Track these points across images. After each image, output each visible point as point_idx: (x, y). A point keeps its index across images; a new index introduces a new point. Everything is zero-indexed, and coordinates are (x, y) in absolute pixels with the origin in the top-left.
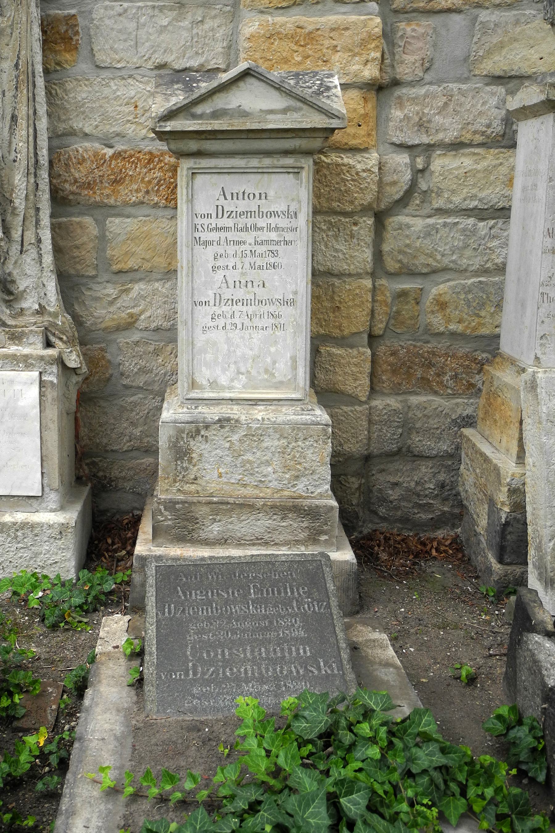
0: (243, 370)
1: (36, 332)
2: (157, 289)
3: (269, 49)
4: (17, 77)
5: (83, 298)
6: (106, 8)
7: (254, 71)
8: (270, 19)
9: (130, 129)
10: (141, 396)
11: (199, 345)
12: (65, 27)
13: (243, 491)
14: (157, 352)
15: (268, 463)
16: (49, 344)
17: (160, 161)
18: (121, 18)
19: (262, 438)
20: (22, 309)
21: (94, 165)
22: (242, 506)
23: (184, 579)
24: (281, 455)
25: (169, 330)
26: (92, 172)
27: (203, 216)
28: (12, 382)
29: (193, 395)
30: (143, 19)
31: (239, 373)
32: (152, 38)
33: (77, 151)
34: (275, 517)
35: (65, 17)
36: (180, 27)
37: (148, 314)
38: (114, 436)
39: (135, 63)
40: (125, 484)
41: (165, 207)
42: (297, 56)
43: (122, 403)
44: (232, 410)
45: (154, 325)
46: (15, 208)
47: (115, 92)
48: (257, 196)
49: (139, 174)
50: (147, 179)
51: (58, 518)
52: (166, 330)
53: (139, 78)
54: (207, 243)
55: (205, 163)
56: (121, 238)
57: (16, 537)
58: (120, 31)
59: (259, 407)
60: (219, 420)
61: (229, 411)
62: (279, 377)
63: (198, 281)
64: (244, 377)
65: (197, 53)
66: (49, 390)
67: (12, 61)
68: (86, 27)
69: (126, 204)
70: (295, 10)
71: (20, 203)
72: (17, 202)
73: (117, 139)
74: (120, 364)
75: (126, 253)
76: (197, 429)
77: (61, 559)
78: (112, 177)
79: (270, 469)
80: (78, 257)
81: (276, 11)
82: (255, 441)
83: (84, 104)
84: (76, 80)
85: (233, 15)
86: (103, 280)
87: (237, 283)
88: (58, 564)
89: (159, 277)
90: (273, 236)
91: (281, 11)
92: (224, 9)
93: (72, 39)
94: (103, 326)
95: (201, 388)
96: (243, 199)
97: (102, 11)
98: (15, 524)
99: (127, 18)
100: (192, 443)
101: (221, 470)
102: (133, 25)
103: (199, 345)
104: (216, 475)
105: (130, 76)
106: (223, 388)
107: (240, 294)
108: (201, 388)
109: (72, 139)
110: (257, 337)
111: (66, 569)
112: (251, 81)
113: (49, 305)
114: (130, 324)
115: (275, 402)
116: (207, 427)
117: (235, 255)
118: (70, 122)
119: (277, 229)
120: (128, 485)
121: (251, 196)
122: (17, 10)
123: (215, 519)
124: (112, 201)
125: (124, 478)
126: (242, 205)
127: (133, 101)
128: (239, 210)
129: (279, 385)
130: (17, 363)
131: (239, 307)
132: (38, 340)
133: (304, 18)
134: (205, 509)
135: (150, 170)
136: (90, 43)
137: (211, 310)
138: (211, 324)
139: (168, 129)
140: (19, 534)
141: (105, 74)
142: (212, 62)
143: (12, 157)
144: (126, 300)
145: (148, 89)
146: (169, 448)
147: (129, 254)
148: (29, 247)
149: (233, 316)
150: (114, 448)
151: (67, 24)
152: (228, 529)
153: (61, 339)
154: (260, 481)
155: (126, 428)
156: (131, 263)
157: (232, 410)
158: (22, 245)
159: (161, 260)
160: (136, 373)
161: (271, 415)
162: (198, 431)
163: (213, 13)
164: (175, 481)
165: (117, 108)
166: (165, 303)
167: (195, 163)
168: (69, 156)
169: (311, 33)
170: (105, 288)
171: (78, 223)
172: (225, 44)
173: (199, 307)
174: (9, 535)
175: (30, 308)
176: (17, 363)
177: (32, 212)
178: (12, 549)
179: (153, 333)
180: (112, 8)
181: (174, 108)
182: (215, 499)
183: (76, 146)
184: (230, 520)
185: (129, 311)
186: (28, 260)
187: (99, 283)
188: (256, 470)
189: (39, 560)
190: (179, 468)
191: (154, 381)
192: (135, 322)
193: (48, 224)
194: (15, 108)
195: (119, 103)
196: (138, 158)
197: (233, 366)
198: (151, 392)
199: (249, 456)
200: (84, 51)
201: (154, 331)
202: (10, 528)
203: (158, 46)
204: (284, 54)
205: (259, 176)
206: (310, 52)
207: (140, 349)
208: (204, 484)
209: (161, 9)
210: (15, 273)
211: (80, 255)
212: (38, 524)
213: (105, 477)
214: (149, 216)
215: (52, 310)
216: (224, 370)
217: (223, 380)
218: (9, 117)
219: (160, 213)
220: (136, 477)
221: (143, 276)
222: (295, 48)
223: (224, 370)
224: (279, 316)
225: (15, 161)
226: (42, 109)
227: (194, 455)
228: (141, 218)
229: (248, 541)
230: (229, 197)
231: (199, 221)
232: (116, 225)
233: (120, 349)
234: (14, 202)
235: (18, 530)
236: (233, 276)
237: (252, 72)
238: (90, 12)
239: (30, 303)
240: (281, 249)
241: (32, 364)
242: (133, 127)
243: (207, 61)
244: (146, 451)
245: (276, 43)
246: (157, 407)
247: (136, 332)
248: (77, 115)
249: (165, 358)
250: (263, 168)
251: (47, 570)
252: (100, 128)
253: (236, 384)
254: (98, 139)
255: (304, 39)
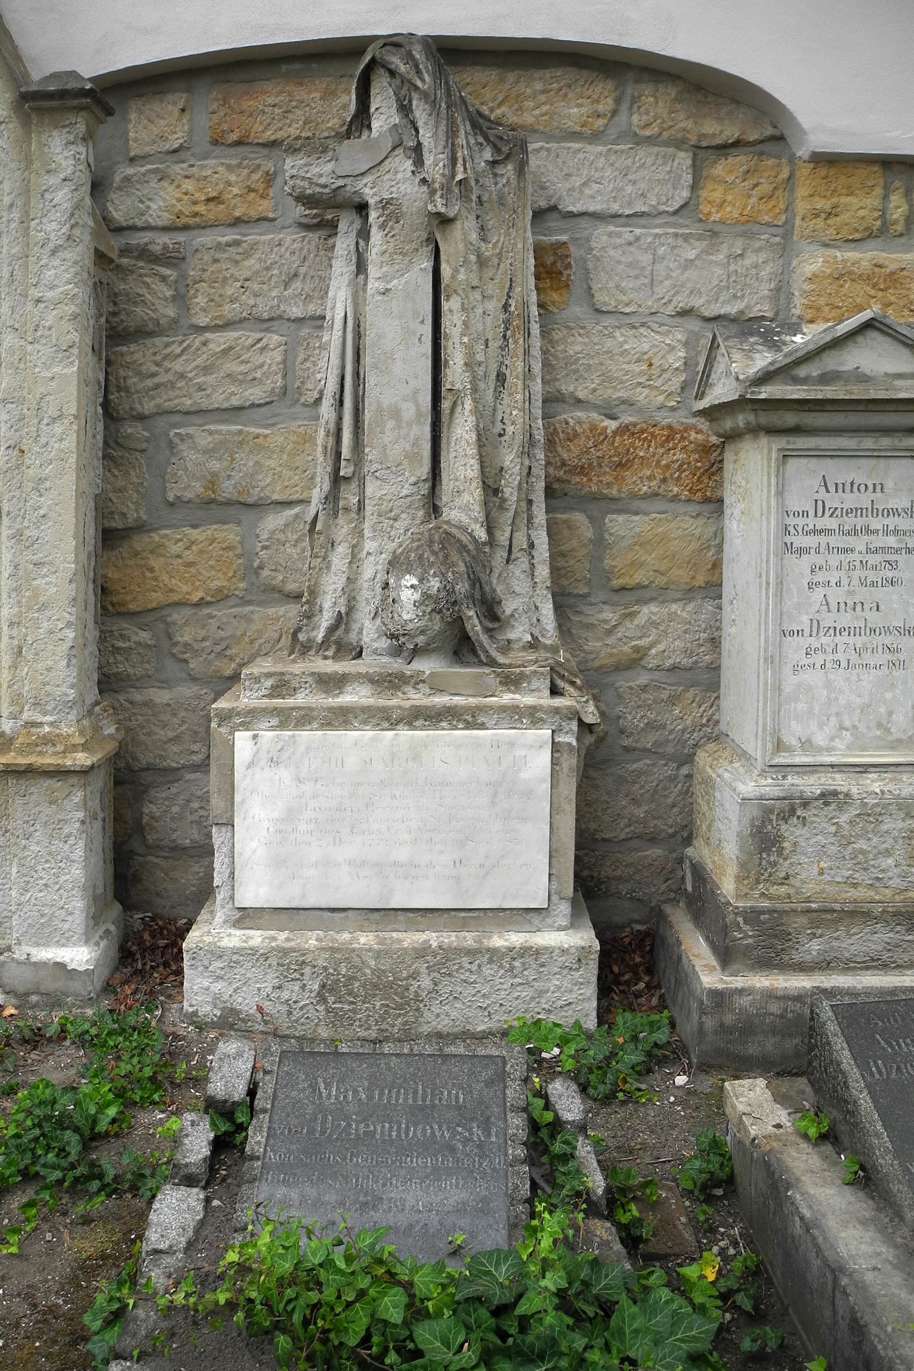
0: (847, 724)
1: (542, 674)
2: (675, 613)
3: (837, 292)
4: (507, 323)
5: (569, 625)
6: (610, 235)
7: (880, 322)
8: (838, 254)
9: (641, 396)
10: (648, 762)
11: (787, 690)
12: (552, 258)
13: (853, 894)
14: (673, 700)
15: (888, 853)
16: (555, 691)
17: (683, 438)
18: (631, 249)
19: (880, 819)
20: (509, 641)
21: (591, 444)
22: (853, 914)
23: (880, 1024)
24: (907, 841)
25: (690, 669)
26: (587, 452)
27: (796, 514)
28: (512, 744)
29: (777, 760)
30: (661, 251)
31: (842, 728)
32: (674, 275)
33: (567, 423)
34: (898, 928)
35: (552, 244)
36: (712, 262)
37: (661, 647)
38: (606, 818)
39: (650, 307)
40: (620, 887)
41: (689, 500)
42: (875, 303)
43: (620, 772)
44: (834, 779)
45: (668, 663)
46: (504, 500)
47: (621, 345)
48: (871, 487)
49: (654, 456)
50: (664, 462)
51: (571, 939)
52: (686, 669)
53: (655, 327)
54: (801, 551)
55: (801, 442)
56: (624, 543)
57: (512, 968)
58: (629, 265)
59: (870, 776)
60: (823, 795)
61: (830, 782)
62: (896, 734)
63: (789, 603)
64: (848, 734)
65: (735, 296)
66: (565, 756)
67: (499, 300)
68: (581, 258)
69: (634, 496)
70: (872, 243)
71: (511, 494)
72: (507, 491)
73: (622, 407)
74: (619, 717)
75: (633, 563)
76: (792, 808)
77: (575, 998)
78: (616, 459)
79: (890, 861)
80: (564, 568)
81: (846, 245)
82: (871, 822)
83: (578, 359)
84: (567, 327)
85: (784, 249)
86: (598, 600)
87: (842, 605)
88: (573, 1006)
89: (678, 596)
90: (892, 541)
91: (852, 245)
92: (771, 241)
93: (561, 273)
94: (597, 664)
95: (789, 749)
96: (852, 491)
97: (605, 238)
98: (511, 949)
99: (639, 248)
100: (784, 827)
101: (822, 864)
102: (646, 258)
103: (787, 690)
104: (816, 871)
105: (643, 325)
106: (820, 750)
107: (845, 619)
108: (789, 749)
109: (558, 407)
110: (868, 678)
111: (584, 1013)
112: (873, 334)
113: (543, 636)
114: (634, 661)
115: (891, 769)
116: (805, 804)
117: (840, 567)
118: (557, 383)
119: (896, 532)
120: (624, 889)
121: (862, 488)
122: (508, 234)
123: (814, 934)
124: (614, 492)
125: (620, 878)
126: (850, 500)
127: (646, 357)
128: (846, 506)
129: (895, 745)
130: (520, 718)
131: (845, 638)
132: (544, 685)
133: (884, 255)
134: (802, 920)
135: (669, 450)
136: (587, 278)
137: (804, 642)
138: (806, 661)
139: (763, 396)
140: (517, 964)
141: (608, 321)
142: (755, 309)
143: (499, 427)
144: (630, 628)
145: (668, 342)
146: (752, 835)
147: (637, 565)
148: (519, 555)
149: (835, 650)
150: (606, 837)
151: (555, 254)
152: (832, 948)
153: (573, 683)
154: (877, 879)
155: (625, 807)
156: (639, 577)
157: (834, 779)
158: (510, 552)
159: (680, 572)
160: (643, 729)
161: (891, 787)
162: (793, 811)
163: (758, 244)
164: (758, 882)
165: (624, 366)
166: (686, 632)
167: (788, 442)
168: (555, 429)
169: (893, 273)
170: (600, 612)
171: (566, 522)
172: (772, 286)
173: (789, 639)
174: (501, 967)
175: (520, 639)
176: (520, 718)
177: (524, 504)
178: (505, 987)
179: (668, 674)
180: (619, 235)
181: (772, 368)
182: (813, 905)
183: (565, 416)
184: (835, 935)
185: (634, 643)
186: (517, 573)
187: (592, 604)
188: (872, 863)
189: (543, 1001)
190: (764, 863)
191: (668, 741)
192: (641, 659)
193: (544, 522)
194: (502, 363)
195: (626, 360)
196: (652, 434)
197: (833, 719)
198: (663, 756)
199: (862, 844)
200: (577, 289)
201: (668, 670)
202: (503, 955)
203: (682, 286)
204: (858, 300)
205: (873, 462)
206: (893, 299)
207: (648, 696)
208: (798, 884)
209: (686, 238)
210: (499, 589)
211: (566, 565)
212: (546, 948)
213: (592, 877)
214: (666, 512)
215: (548, 642)
216: (821, 725)
217: (820, 739)
218: (493, 376)
219: (681, 508)
220: (637, 877)
221: (654, 595)
222: (873, 292)
223: (821, 725)
224: (898, 650)
225: (500, 435)
226: (537, 367)
227: (785, 845)
228: (654, 515)
229: (859, 963)
230: (832, 489)
231: (791, 521)
232: (619, 525)
233: (619, 696)
234: (502, 492)
235: (514, 959)
236: (836, 595)
237: (876, 324)
238: (588, 239)
239: (519, 633)
240: (902, 558)
241: (541, 719)
242: (646, 391)
243: (748, 307)
244: (652, 840)
245: (847, 286)
246: (670, 776)
247: (642, 672)
248: (567, 375)
249: (683, 708)
250: (880, 450)
251: (556, 1015)
252: (599, 392)
253: (838, 743)
254: (595, 407)
255: (885, 281)
